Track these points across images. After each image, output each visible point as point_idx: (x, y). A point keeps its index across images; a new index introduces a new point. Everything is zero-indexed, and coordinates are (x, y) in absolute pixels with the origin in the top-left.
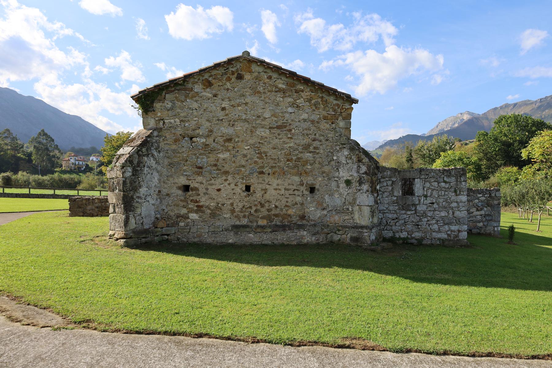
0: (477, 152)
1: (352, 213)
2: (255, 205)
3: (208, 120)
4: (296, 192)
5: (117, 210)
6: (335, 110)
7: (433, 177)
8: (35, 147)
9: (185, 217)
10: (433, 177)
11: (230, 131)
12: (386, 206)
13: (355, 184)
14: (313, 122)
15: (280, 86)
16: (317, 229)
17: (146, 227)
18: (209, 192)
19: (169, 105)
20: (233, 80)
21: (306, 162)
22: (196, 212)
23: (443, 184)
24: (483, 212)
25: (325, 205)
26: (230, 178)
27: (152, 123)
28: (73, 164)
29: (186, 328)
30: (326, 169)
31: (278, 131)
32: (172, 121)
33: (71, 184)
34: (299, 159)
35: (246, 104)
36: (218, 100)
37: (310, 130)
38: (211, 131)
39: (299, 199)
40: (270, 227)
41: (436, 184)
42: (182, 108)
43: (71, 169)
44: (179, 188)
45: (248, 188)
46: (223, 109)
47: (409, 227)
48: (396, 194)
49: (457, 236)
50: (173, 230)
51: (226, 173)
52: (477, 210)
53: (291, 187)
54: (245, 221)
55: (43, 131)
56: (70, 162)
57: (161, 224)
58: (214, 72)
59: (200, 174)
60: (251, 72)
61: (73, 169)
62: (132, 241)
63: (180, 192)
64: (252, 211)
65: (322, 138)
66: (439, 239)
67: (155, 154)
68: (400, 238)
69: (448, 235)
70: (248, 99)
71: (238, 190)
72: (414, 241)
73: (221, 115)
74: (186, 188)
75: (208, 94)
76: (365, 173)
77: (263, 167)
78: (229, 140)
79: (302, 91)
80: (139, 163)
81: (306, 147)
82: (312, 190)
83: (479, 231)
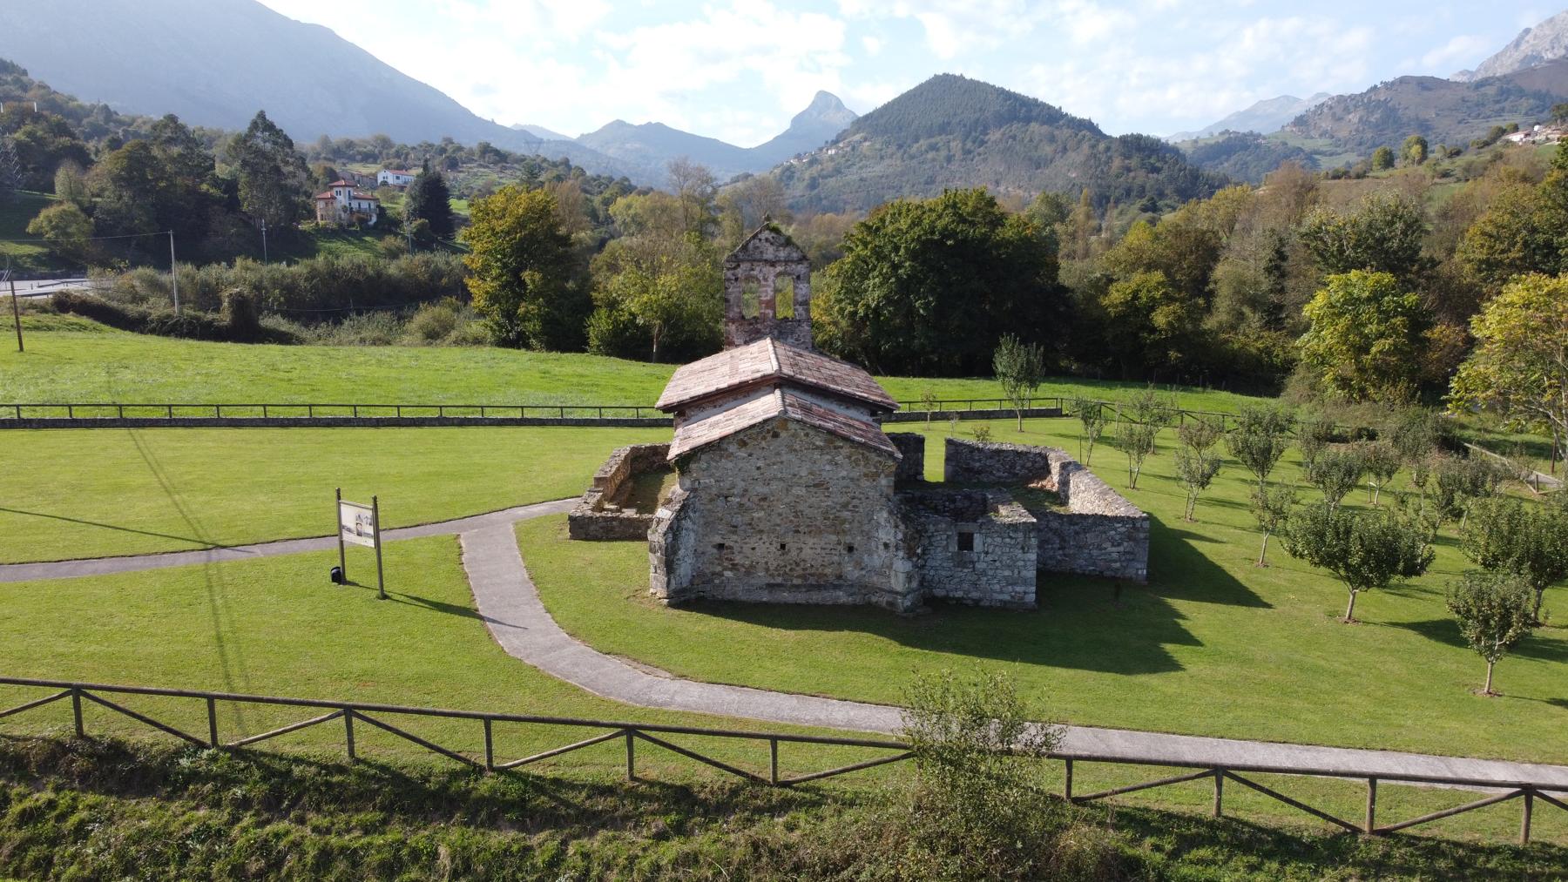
0: (1549, 203)
1: (889, 577)
2: (791, 564)
3: (743, 480)
4: (833, 552)
5: (659, 571)
6: (876, 467)
7: (997, 532)
8: (245, 164)
9: (720, 575)
10: (997, 532)
11: (765, 490)
12: (939, 562)
13: (892, 549)
14: (852, 479)
15: (817, 443)
16: (853, 590)
17: (684, 585)
18: (744, 550)
19: (705, 466)
20: (769, 438)
21: (844, 521)
22: (731, 570)
23: (1008, 540)
24: (1121, 549)
25: (863, 565)
26: (764, 537)
27: (688, 483)
28: (345, 209)
29: (736, 682)
30: (866, 528)
31: (815, 490)
32: (707, 481)
33: (358, 282)
34: (837, 518)
35: (782, 463)
36: (753, 460)
37: (848, 487)
38: (746, 490)
39: (836, 558)
40: (805, 586)
41: (999, 540)
42: (717, 468)
43: (341, 225)
44: (714, 547)
45: (783, 546)
46: (759, 468)
47: (966, 586)
48: (951, 549)
49: (1022, 598)
50: (708, 588)
51: (761, 532)
52: (1113, 546)
53: (828, 546)
54: (779, 580)
55: (262, 115)
56: (338, 205)
57: (696, 581)
58: (749, 432)
59: (734, 533)
60: (787, 429)
61: (345, 223)
62: (673, 601)
63: (715, 551)
64: (787, 570)
65: (861, 496)
66: (1001, 601)
67: (691, 515)
68: (954, 598)
69: (1012, 597)
70: (784, 458)
71: (773, 549)
72: (969, 602)
73: (756, 474)
74: (721, 546)
75: (742, 453)
76: (901, 540)
77: (798, 526)
78: (764, 499)
79: (842, 447)
80: (678, 527)
81: (845, 506)
82: (850, 549)
83: (1113, 574)
